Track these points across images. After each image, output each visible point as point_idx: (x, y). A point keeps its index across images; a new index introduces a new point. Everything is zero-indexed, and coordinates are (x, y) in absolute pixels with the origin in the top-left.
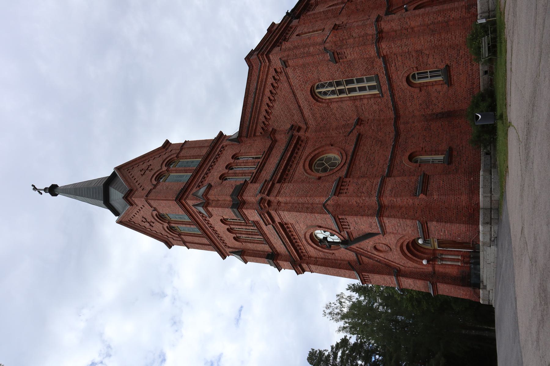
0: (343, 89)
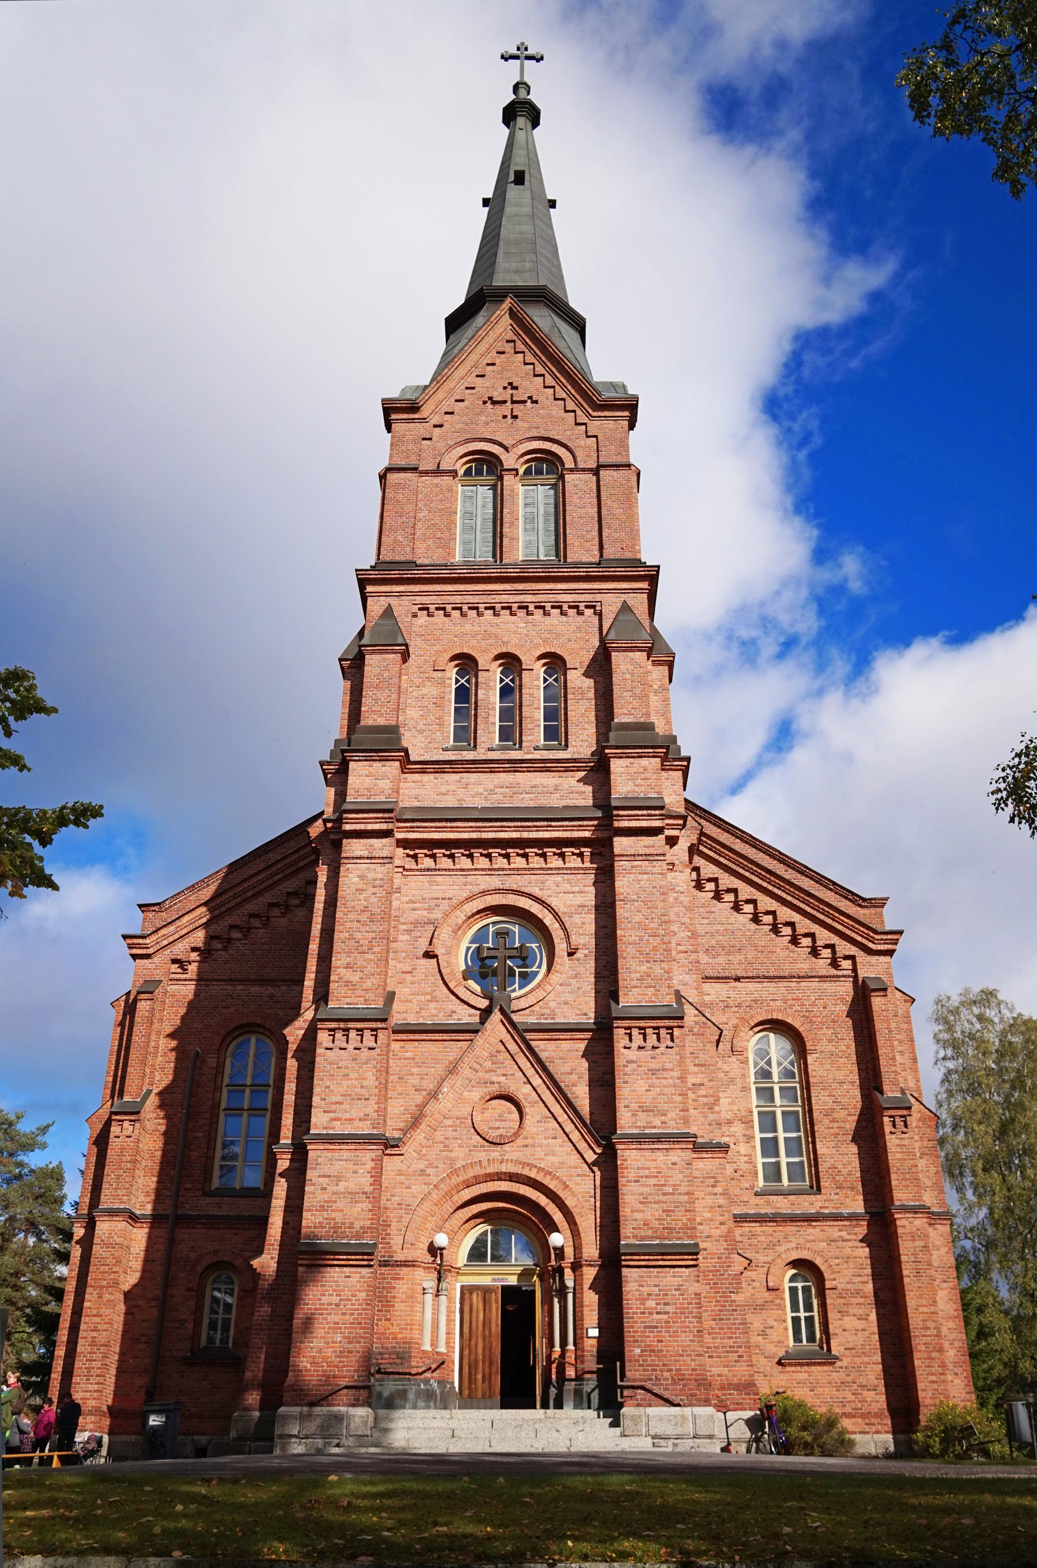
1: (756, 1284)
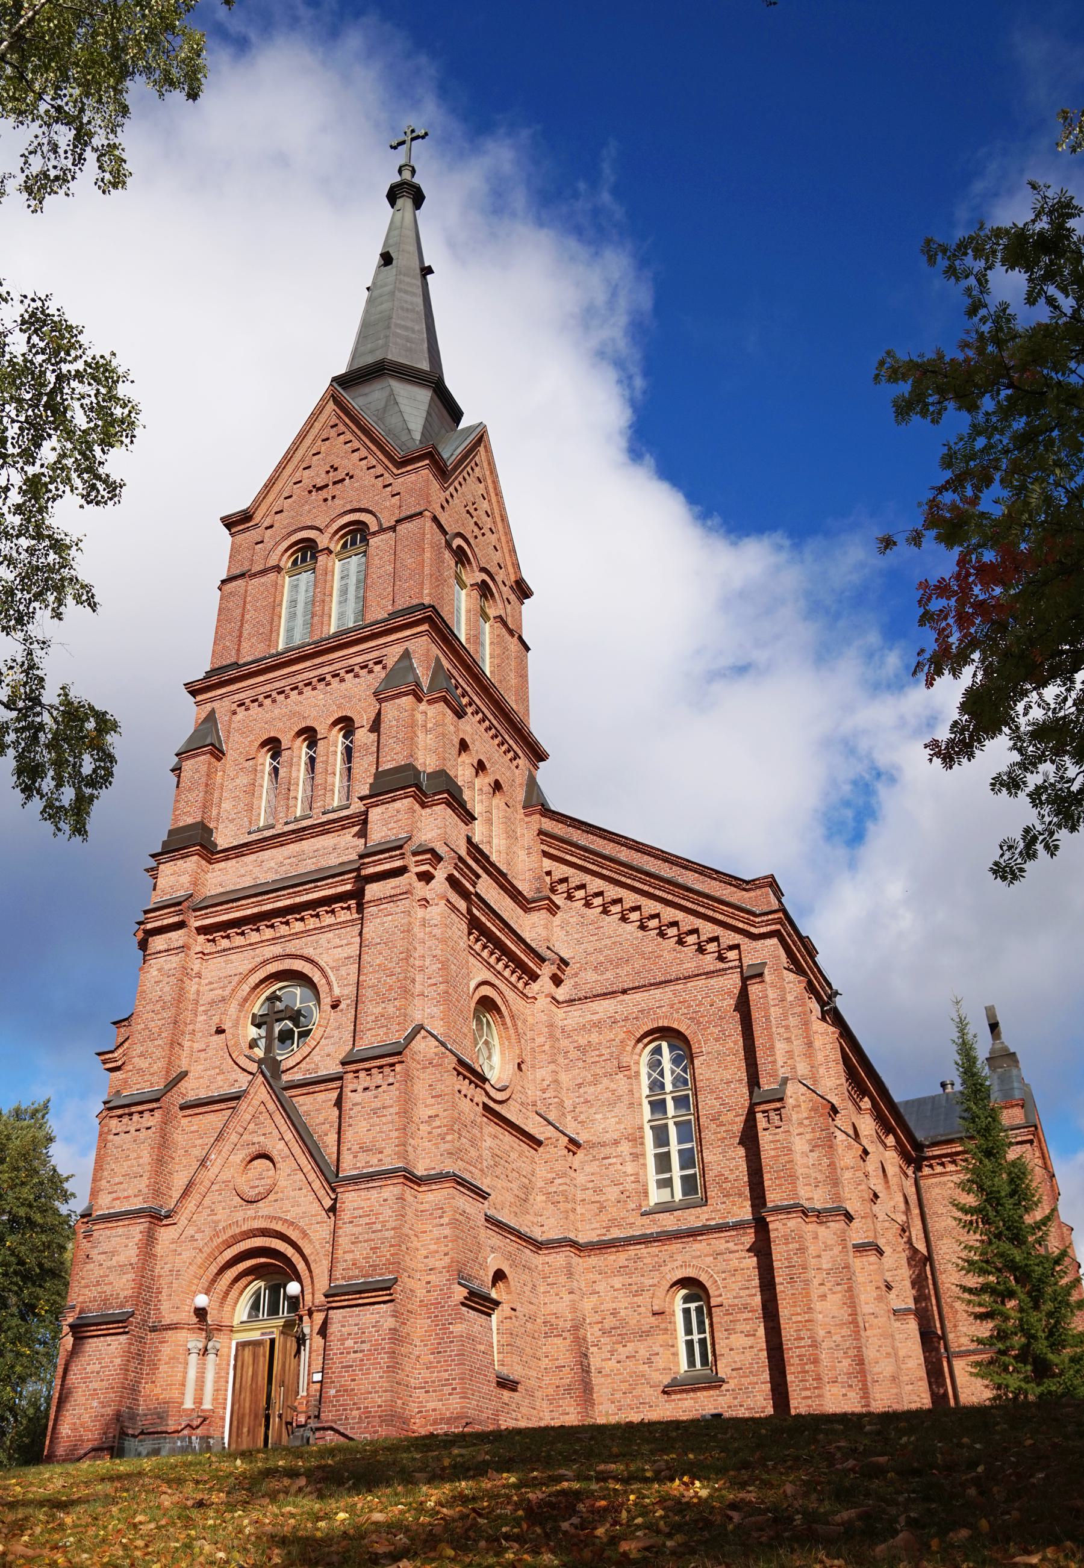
0: (665, 1113)
1: (642, 1310)
